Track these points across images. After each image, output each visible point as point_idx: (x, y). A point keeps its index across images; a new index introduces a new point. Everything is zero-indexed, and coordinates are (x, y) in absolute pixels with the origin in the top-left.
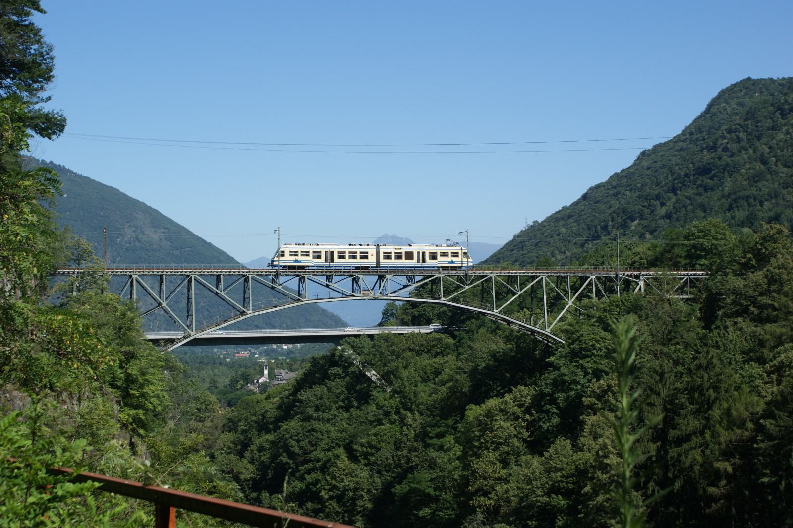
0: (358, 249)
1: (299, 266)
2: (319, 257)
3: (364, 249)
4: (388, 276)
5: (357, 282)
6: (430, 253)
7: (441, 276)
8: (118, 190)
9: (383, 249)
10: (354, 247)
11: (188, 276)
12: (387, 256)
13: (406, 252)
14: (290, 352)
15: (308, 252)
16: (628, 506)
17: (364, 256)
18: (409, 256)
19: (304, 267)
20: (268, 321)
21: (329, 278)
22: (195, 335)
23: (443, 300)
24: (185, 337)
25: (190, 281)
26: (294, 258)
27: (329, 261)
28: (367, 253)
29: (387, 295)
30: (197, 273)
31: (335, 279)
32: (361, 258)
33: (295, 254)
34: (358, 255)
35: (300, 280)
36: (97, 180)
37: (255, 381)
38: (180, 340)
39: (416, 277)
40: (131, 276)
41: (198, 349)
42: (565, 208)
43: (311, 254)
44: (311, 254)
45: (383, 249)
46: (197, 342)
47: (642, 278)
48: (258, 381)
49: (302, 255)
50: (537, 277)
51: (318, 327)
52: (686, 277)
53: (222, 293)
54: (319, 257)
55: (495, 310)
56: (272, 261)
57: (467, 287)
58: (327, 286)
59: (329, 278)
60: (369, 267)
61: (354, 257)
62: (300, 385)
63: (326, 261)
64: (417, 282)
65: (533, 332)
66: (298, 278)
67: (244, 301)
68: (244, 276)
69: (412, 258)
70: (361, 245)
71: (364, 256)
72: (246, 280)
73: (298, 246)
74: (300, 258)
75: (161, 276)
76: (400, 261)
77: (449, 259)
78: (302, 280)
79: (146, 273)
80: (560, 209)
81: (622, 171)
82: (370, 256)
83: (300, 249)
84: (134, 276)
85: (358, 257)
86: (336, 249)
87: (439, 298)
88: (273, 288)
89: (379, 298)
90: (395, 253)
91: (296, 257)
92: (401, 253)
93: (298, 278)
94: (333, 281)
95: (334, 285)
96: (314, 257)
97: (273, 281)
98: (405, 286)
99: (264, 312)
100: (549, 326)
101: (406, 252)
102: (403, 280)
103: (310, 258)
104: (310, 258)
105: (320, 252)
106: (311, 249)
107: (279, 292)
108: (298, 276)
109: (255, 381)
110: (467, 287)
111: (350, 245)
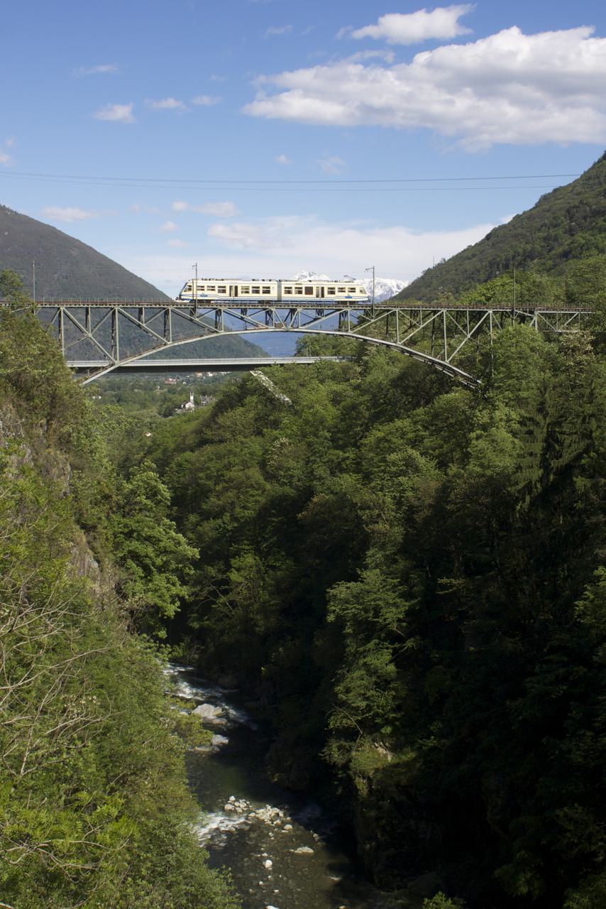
0: (261, 285)
1: (350, 302)
2: (224, 291)
3: (266, 284)
4: (299, 310)
5: (270, 315)
6: (329, 288)
7: (397, 311)
8: (55, 228)
9: (284, 285)
10: (257, 282)
11: (112, 309)
12: (288, 291)
13: (306, 288)
14: (214, 379)
15: (214, 287)
16: (389, 658)
17: (267, 291)
18: (309, 290)
19: (355, 302)
20: (173, 353)
21: (244, 311)
22: (118, 364)
23: (350, 333)
24: (112, 365)
25: (114, 313)
26: (200, 292)
27: (320, 296)
28: (269, 288)
29: (298, 328)
30: (121, 306)
31: (249, 312)
32: (264, 292)
33: (202, 288)
34: (261, 290)
35: (217, 312)
36: (36, 219)
37: (182, 406)
38: (104, 368)
39: (325, 311)
40: (59, 308)
41: (129, 378)
42: (470, 248)
43: (217, 289)
44: (217, 289)
45: (284, 285)
46: (121, 370)
47: (536, 313)
48: (184, 406)
49: (208, 290)
50: (439, 311)
51: (187, 358)
52: (577, 313)
53: (144, 325)
54: (224, 291)
55: (398, 343)
56: (180, 295)
57: (373, 321)
58: (242, 319)
59: (244, 311)
60: (272, 301)
61: (257, 292)
62: (220, 408)
63: (317, 296)
64: (326, 316)
65: (433, 362)
66: (214, 311)
67: (165, 332)
68: (165, 308)
69: (312, 293)
70: (263, 280)
71: (267, 291)
72: (167, 313)
73: (204, 281)
74: (206, 292)
75: (87, 309)
76: (300, 295)
77: (346, 294)
78: (218, 313)
79: (73, 306)
80: (465, 248)
81: (524, 213)
82: (271, 290)
83: (206, 284)
84: (62, 309)
85: (261, 292)
86: (240, 284)
87: (347, 331)
88: (191, 320)
89: (291, 330)
90: (296, 288)
91: (203, 292)
92: (301, 288)
93: (214, 311)
94: (248, 314)
95: (249, 318)
96: (219, 291)
97: (192, 314)
98: (316, 319)
99: (183, 343)
100: (448, 358)
101: (306, 288)
102: (313, 314)
103: (216, 292)
104: (216, 292)
105: (225, 287)
106: (217, 284)
107: (196, 323)
108: (214, 309)
109: (182, 406)
110: (373, 321)
111: (253, 280)
